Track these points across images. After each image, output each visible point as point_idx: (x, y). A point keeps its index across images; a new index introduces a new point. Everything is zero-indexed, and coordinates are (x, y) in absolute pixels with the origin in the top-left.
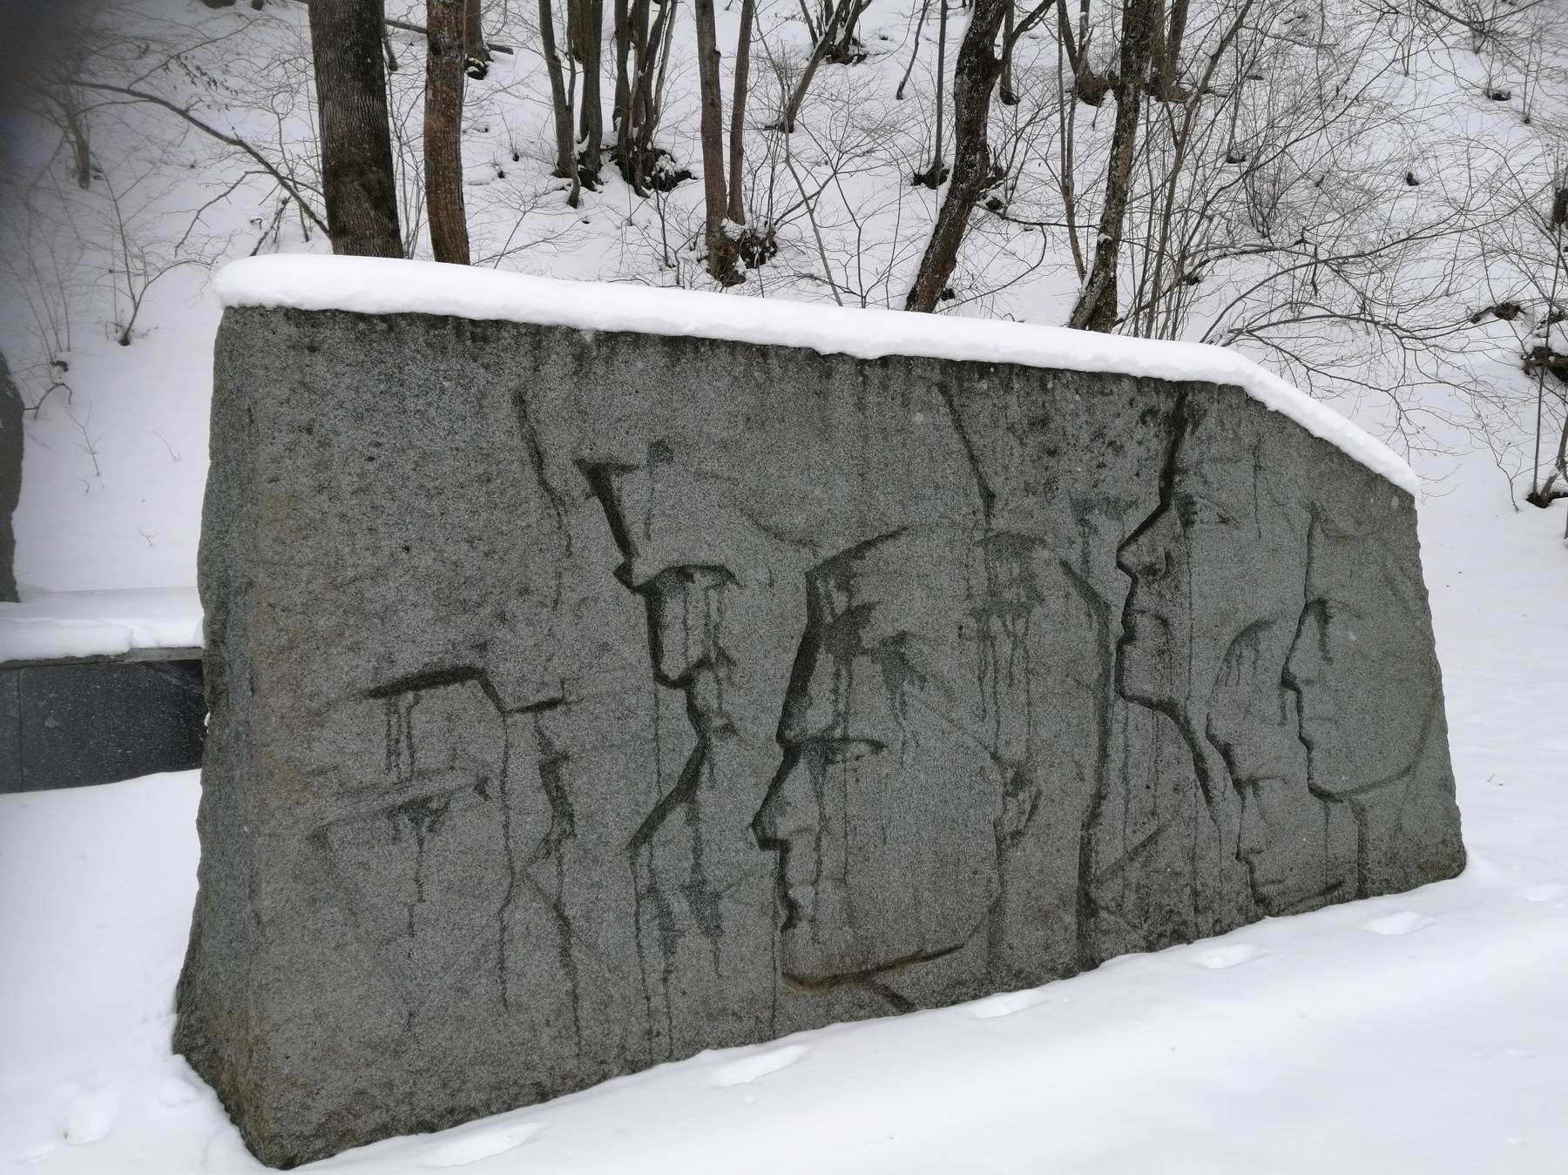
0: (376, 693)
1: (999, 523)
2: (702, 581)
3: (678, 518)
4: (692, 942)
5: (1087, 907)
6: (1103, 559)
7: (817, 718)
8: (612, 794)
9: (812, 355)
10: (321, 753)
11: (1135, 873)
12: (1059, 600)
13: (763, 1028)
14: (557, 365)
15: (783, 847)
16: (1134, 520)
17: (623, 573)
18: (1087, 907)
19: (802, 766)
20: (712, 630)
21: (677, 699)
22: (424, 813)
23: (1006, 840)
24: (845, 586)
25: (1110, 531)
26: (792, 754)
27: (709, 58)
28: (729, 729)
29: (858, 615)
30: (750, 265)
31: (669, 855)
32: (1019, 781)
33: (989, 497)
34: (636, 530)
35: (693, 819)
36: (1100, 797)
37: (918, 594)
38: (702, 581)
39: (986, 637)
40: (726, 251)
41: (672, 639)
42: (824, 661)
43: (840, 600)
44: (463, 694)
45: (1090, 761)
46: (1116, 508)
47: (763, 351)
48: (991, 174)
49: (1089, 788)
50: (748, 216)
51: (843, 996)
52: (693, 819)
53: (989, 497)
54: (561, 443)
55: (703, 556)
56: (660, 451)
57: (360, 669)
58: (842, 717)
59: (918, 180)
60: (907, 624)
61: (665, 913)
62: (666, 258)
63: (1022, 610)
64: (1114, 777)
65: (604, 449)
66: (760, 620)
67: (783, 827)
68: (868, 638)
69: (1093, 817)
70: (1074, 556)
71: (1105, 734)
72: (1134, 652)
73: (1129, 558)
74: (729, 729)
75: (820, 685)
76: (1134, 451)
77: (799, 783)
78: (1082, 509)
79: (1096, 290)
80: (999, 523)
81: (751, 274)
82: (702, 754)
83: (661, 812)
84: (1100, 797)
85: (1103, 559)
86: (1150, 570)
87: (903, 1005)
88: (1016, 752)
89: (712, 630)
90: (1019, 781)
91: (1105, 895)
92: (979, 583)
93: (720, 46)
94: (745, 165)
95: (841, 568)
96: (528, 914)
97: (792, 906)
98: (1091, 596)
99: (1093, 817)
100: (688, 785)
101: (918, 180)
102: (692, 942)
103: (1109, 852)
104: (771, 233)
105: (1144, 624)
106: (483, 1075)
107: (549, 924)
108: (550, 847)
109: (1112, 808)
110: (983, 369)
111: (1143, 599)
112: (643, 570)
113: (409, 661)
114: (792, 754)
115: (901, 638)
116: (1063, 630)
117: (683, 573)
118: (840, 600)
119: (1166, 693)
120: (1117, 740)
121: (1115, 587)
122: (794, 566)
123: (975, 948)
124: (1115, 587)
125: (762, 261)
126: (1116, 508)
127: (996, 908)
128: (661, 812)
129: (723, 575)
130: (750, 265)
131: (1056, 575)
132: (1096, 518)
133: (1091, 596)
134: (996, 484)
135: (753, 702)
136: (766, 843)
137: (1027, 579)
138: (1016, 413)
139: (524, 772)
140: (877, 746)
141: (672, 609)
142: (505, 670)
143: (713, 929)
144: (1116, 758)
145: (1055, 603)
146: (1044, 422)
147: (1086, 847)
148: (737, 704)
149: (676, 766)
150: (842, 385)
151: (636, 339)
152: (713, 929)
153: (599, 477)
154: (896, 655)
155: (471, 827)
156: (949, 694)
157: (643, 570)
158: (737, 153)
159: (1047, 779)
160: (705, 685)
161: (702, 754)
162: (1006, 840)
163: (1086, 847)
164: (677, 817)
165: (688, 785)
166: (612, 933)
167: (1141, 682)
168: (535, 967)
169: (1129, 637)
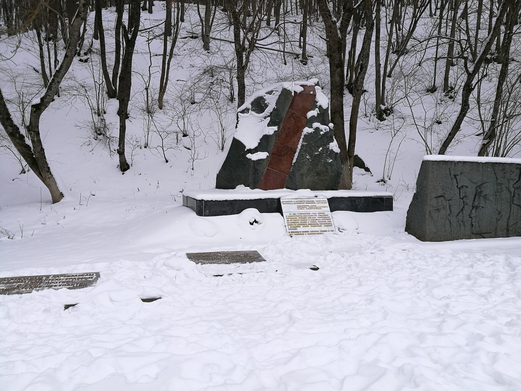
0: (436, 198)
1: (498, 182)
2: (464, 187)
3: (463, 181)
4: (462, 227)
5: (508, 230)
6: (511, 186)
7: (476, 204)
8: (455, 210)
9: (477, 162)
10: (432, 203)
11: (514, 226)
12: (505, 191)
13: (469, 238)
14: (453, 165)
15: (472, 218)
16: (515, 182)
17: (457, 186)
18: (508, 230)
19: (474, 209)
20: (465, 193)
21: (462, 200)
22: (438, 210)
23: (498, 220)
24: (480, 189)
25: (512, 183)
26: (473, 208)
27: (378, 65)
28: (467, 204)
29: (481, 192)
30: (387, 116)
31: (460, 217)
32: (499, 213)
33: (497, 178)
34: (458, 182)
35: (463, 214)
36: (510, 216)
37: (488, 190)
38: (464, 187)
39: (496, 195)
40: (381, 113)
41: (461, 194)
42: (477, 197)
43: (479, 190)
44: (442, 198)
45: (509, 211)
46: (513, 180)
47: (473, 162)
48: (449, 89)
49: (508, 215)
50: (386, 104)
51: (478, 236)
52: (463, 214)
53: (497, 178)
54: (453, 173)
55: (465, 185)
56: (461, 173)
57: (435, 195)
58: (479, 204)
59: (428, 91)
60: (487, 193)
61: (460, 224)
62: (366, 115)
63: (501, 192)
64: (512, 214)
65: (457, 173)
66: (470, 191)
67: (472, 216)
68: (482, 195)
69: (509, 219)
70: (507, 186)
71: (511, 208)
72: (515, 198)
73: (514, 186)
74: (467, 204)
75: (476, 200)
76: (515, 173)
77: (474, 211)
78: (508, 180)
79: (491, 131)
80: (498, 182)
81: (387, 118)
82: (464, 207)
83: (459, 213)
84: (510, 216)
85: (511, 186)
86: (517, 188)
87: (484, 238)
88: (500, 210)
89: (465, 193)
90: (499, 213)
91: (510, 229)
92: (496, 189)
93: (381, 62)
94: (386, 91)
95: (479, 186)
96: (447, 222)
97: (472, 225)
98: (509, 191)
99: (509, 219)
100: (462, 210)
101: (428, 91)
102: (462, 227)
103: (511, 224)
104: (392, 108)
105: (516, 195)
106: (443, 237)
107: (449, 223)
108: (449, 215)
109: (511, 218)
110: (497, 163)
111: (516, 191)
112: (459, 186)
113: (439, 195)
114: (473, 208)
115: (486, 195)
116: (505, 195)
117: (462, 187)
118: (479, 190)
119: (519, 204)
120: (512, 209)
121: (512, 190)
122: (474, 186)
123: (493, 233)
124: (512, 190)
125: (389, 114)
126: (513, 180)
127: (496, 228)
128: (459, 213)
129: (467, 187)
130: (387, 116)
131: (505, 188)
132: (510, 181)
133: (509, 191)
134: (498, 177)
135: (470, 201)
136: (470, 217)
137: (501, 189)
138: (500, 168)
139: (448, 207)
140: (483, 207)
141: (461, 190)
142: (446, 196)
143: (464, 226)
144: (512, 212)
145: (505, 191)
146: (504, 170)
147: (508, 223)
148: (468, 201)
149: (461, 208)
150: (481, 166)
151: (460, 162)
152: (464, 226)
153: (455, 176)
154: (485, 197)
155: (443, 212)
156: (491, 202)
157: (459, 186)
158: (384, 88)
159: (503, 213)
160: (464, 199)
161: (464, 207)
162: (498, 220)
163: (508, 223)
164: (461, 213)
165: (462, 210)
166: (455, 225)
167: (516, 202)
168: (448, 227)
169: (514, 196)
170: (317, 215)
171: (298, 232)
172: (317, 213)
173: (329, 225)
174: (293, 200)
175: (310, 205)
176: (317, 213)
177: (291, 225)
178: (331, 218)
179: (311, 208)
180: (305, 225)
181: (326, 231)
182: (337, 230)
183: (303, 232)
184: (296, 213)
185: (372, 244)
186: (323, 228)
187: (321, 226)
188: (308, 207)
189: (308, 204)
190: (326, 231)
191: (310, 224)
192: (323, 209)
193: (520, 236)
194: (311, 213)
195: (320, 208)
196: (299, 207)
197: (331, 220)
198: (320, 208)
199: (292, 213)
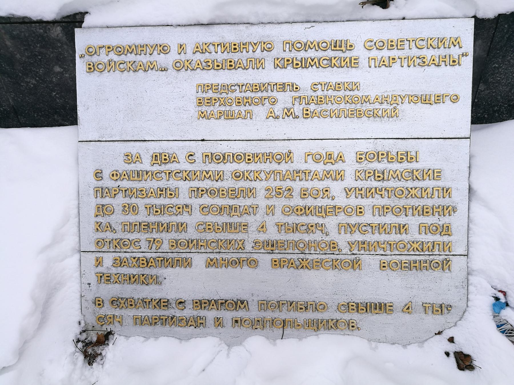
170: (350, 167)
171: (162, 303)
172: (350, 150)
173: (432, 257)
174: (172, 38)
175: (305, 78)
176: (350, 150)
177: (120, 244)
178: (459, 197)
179: (312, 106)
180: (229, 255)
181: (381, 307)
182: (482, 303)
183: (200, 304)
184: (180, 150)
185: (99, 226)
186: (392, 287)
187: (355, 264)
188: (284, 99)
189: (289, 75)
190: (381, 307)
191: (271, 246)
192: (417, 119)
193: (513, 119)
194: (298, 149)
195: (389, 107)
196: (213, 103)
197: (457, 221)
198: (389, 107)
199: (146, 151)
